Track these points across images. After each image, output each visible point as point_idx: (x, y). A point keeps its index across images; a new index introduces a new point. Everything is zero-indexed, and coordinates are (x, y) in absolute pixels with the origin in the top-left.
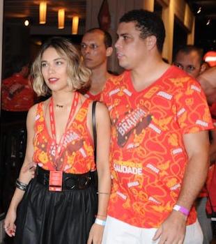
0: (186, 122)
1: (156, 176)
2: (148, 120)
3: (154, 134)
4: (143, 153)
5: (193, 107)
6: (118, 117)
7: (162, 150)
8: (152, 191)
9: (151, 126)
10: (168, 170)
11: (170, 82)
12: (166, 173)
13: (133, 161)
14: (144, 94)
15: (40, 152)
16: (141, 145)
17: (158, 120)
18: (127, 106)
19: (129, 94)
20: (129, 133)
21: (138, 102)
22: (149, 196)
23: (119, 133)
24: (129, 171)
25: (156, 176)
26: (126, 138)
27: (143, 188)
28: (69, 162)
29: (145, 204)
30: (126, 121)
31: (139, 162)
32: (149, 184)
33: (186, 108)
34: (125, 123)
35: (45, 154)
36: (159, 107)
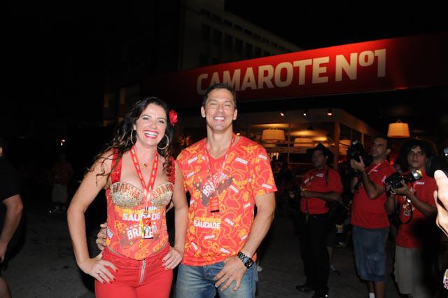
2: (229, 182)
3: (233, 192)
5: (260, 172)
6: (201, 180)
8: (225, 243)
10: (240, 223)
22: (221, 247)
31: (219, 218)
32: (230, 197)
34: (208, 186)
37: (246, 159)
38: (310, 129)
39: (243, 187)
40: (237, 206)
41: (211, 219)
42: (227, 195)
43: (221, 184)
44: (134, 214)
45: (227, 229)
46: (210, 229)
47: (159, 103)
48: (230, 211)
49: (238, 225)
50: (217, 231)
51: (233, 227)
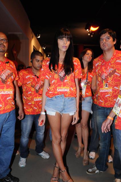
2: (114, 71)
3: (117, 76)
6: (34, 84)
15: (55, 74)
17: (119, 71)
21: (108, 65)
22: (114, 99)
26: (64, 78)
27: (112, 96)
28: (67, 78)
29: (112, 102)
31: (111, 87)
34: (4, 74)
35: (57, 75)
36: (118, 66)
41: (65, 87)
42: (114, 77)
43: (110, 72)
44: (3, 91)
46: (107, 92)
47: (90, 50)
48: (116, 83)
50: (111, 93)
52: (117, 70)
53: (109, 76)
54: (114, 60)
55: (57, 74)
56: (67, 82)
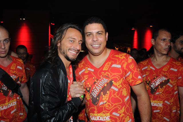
0: (133, 78)
1: (117, 118)
3: (114, 92)
4: (109, 106)
6: (150, 80)
7: (120, 101)
9: (113, 87)
10: (124, 113)
11: (115, 57)
12: (123, 115)
13: (104, 113)
14: (103, 69)
16: (107, 101)
18: (94, 78)
19: (154, 69)
20: (99, 95)
21: (100, 74)
23: (92, 96)
24: (155, 105)
25: (117, 118)
26: (98, 98)
28: (103, 99)
30: (96, 88)
31: (108, 113)
33: (131, 70)
34: (95, 89)
37: (29, 69)
38: (60, 27)
39: (121, 86)
40: (120, 101)
42: (110, 93)
45: (167, 107)
49: (172, 104)
51: (119, 117)
52: (171, 80)
53: (102, 93)
54: (109, 64)
55: (149, 85)
56: (103, 104)
